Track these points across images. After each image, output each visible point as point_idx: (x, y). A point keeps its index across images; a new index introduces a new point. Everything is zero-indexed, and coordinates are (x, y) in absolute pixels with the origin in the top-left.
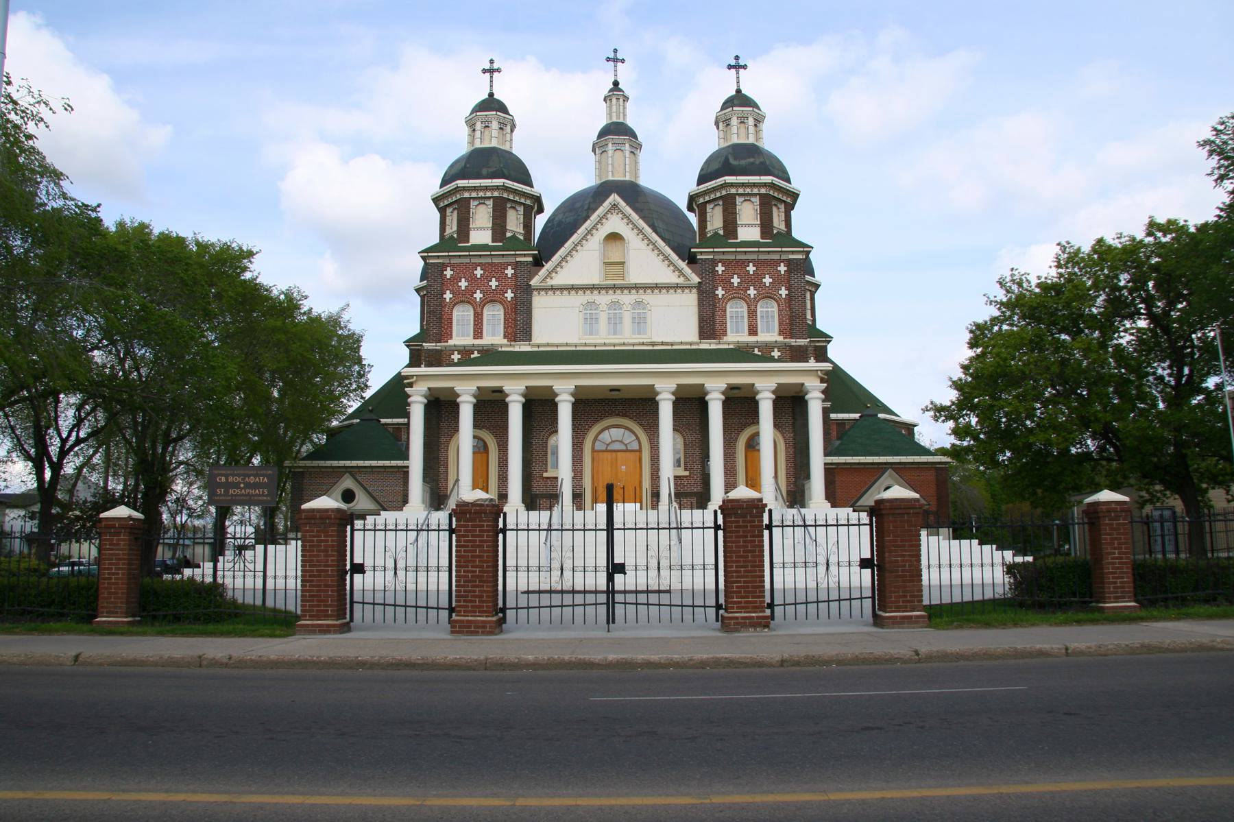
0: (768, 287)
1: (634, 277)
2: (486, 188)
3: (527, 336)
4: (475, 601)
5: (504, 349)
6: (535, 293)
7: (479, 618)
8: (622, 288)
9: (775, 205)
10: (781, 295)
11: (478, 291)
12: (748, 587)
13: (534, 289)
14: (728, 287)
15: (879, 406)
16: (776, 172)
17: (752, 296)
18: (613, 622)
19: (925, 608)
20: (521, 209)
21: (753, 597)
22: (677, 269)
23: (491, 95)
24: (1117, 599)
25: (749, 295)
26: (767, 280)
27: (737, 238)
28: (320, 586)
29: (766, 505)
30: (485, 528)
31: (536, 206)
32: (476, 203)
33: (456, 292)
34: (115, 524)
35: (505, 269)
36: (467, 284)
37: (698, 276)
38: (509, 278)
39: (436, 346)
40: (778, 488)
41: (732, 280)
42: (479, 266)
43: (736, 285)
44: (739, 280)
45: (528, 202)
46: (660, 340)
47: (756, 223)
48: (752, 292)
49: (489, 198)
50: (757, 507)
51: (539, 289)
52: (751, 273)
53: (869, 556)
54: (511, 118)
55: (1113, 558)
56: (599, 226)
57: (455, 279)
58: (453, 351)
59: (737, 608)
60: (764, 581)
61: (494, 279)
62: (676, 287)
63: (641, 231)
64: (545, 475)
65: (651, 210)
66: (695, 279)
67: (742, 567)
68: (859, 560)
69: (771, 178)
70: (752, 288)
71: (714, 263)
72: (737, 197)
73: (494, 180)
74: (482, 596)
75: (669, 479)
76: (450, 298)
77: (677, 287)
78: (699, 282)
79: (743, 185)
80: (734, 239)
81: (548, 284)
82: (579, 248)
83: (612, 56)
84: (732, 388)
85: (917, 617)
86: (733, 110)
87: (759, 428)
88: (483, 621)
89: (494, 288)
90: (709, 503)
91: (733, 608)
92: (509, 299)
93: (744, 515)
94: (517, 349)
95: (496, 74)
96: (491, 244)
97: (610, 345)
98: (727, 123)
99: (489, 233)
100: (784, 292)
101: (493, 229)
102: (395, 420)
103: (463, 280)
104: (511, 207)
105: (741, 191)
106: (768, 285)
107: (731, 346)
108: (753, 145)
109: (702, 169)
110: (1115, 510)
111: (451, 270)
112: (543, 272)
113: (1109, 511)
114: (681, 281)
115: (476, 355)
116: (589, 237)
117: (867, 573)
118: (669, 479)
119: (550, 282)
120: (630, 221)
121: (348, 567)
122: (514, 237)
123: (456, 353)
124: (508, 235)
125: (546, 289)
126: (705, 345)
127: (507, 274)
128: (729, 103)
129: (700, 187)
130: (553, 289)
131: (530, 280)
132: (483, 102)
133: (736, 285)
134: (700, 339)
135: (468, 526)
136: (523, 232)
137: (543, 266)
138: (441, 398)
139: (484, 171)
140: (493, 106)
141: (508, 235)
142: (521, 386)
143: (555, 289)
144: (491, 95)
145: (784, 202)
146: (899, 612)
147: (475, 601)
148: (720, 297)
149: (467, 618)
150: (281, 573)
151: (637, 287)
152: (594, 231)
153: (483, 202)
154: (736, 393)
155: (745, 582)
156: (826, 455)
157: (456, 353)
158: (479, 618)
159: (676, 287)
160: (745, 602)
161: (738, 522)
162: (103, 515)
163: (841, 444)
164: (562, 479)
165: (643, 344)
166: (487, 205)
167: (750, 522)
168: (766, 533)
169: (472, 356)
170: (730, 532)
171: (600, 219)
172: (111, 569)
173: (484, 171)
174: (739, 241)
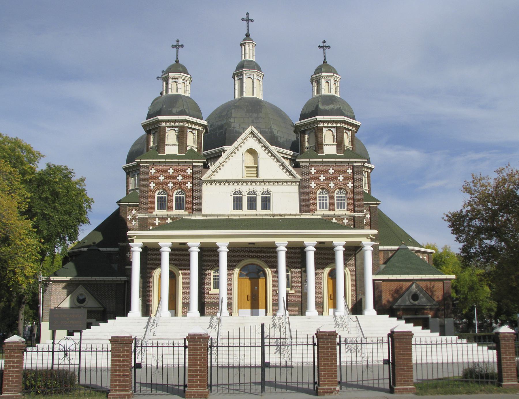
0: (341, 182)
4: (197, 382)
5: (186, 217)
7: (199, 391)
9: (345, 132)
10: (349, 187)
11: (171, 183)
12: (329, 374)
13: (204, 182)
14: (318, 182)
15: (410, 241)
16: (346, 113)
17: (332, 187)
18: (264, 391)
19: (415, 384)
20: (195, 132)
21: (331, 379)
22: (288, 171)
23: (177, 62)
25: (330, 186)
26: (341, 178)
27: (323, 153)
28: (120, 375)
29: (338, 334)
30: (202, 349)
31: (204, 130)
33: (157, 182)
34: (13, 345)
36: (164, 178)
37: (300, 176)
38: (189, 175)
39: (145, 215)
40: (346, 304)
41: (320, 178)
42: (171, 167)
43: (322, 180)
44: (343, 178)
45: (200, 128)
46: (278, 213)
47: (334, 143)
48: (332, 185)
50: (333, 335)
51: (207, 182)
52: (331, 173)
53: (387, 358)
54: (190, 76)
55: (506, 360)
56: (242, 145)
57: (157, 175)
59: (324, 384)
60: (336, 361)
61: (180, 176)
62: (287, 182)
64: (210, 292)
65: (269, 118)
66: (299, 177)
67: (326, 364)
68: (382, 360)
69: (344, 117)
70: (332, 182)
71: (310, 168)
72: (323, 128)
73: (180, 116)
74: (201, 380)
75: (283, 298)
76: (154, 187)
77: (288, 182)
78: (301, 179)
79: (327, 122)
80: (321, 153)
81: (212, 179)
82: (230, 157)
83: (245, 17)
84: (320, 243)
85: (410, 389)
86: (321, 75)
87: (335, 266)
88: (201, 392)
89: (180, 181)
90: (307, 311)
91: (322, 384)
92: (189, 188)
93: (327, 339)
94: (194, 218)
95: (180, 49)
96: (178, 154)
97: (248, 215)
98: (319, 82)
99: (177, 148)
100: (350, 185)
102: (109, 249)
103: (161, 176)
104: (190, 132)
105: (326, 125)
106: (341, 180)
107: (320, 217)
108: (333, 96)
109: (303, 110)
110: (507, 337)
111: (154, 170)
112: (209, 172)
113: (504, 337)
114: (290, 178)
115: (169, 221)
116: (236, 151)
118: (283, 298)
119: (213, 178)
120: (261, 142)
121: (133, 365)
122: (191, 150)
123: (157, 219)
124: (188, 148)
125: (211, 182)
126: (304, 216)
127: (188, 173)
128: (319, 70)
129: (302, 121)
130: (215, 182)
131: (202, 177)
132: (172, 66)
133: (322, 180)
134: (300, 212)
135: (194, 345)
136: (197, 147)
137: (209, 168)
138: (148, 247)
139: (174, 110)
140: (179, 69)
141: (188, 148)
143: (216, 182)
144: (177, 62)
145: (351, 130)
146: (402, 386)
147: (197, 382)
148: (313, 187)
149: (193, 390)
151: (264, 182)
152: (239, 147)
153: (173, 128)
154: (321, 245)
155: (328, 371)
156: (373, 274)
157: (157, 219)
158: (199, 391)
159: (287, 182)
160: (328, 381)
161: (324, 342)
162: (7, 340)
163: (385, 267)
164: (222, 298)
165: (268, 215)
167: (330, 342)
168: (338, 347)
169: (167, 221)
170: (320, 347)
171: (243, 141)
174: (324, 154)
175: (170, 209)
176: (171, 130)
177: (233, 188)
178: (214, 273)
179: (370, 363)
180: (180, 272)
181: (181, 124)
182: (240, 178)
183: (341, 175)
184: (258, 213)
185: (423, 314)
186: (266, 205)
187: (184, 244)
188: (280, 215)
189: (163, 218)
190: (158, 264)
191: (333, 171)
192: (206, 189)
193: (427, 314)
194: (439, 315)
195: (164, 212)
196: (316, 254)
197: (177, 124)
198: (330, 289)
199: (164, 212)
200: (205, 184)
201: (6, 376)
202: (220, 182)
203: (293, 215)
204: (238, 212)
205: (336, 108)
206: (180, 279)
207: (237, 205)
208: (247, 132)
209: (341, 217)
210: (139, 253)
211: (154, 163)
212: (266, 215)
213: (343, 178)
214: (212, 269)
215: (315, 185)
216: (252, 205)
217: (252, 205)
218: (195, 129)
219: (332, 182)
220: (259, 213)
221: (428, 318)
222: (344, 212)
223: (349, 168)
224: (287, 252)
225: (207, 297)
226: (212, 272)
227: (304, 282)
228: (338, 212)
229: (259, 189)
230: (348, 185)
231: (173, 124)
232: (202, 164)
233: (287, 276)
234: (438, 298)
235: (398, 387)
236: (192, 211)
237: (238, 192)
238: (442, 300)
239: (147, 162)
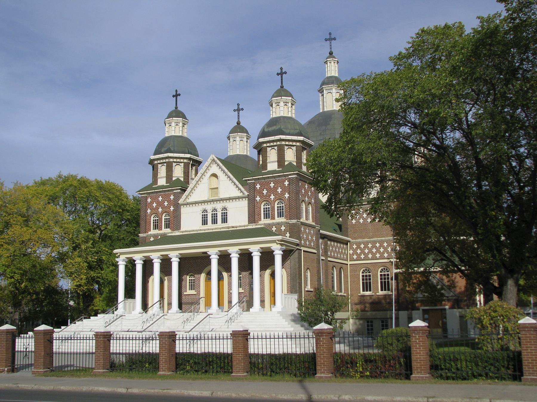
1: (222, 196)
2: (273, 141)
3: (178, 227)
5: (170, 235)
6: (182, 206)
8: (216, 201)
17: (272, 199)
20: (294, 148)
24: (238, 372)
26: (279, 190)
32: (176, 164)
35: (284, 182)
44: (281, 190)
45: (185, 161)
49: (182, 162)
51: (183, 205)
58: (151, 236)
62: (239, 198)
63: (224, 172)
82: (199, 182)
96: (277, 170)
97: (210, 229)
101: (278, 161)
107: (262, 226)
115: (152, 239)
117: (91, 346)
119: (188, 201)
122: (178, 179)
134: (249, 222)
139: (163, 150)
142: (236, 248)
150: (57, 347)
159: (239, 198)
172: (533, 371)
173: (163, 150)
175: (273, 218)
176: (272, 149)
177: (200, 208)
178: (190, 277)
179: (137, 352)
180: (166, 278)
181: (278, 143)
182: (206, 198)
183: (279, 188)
184: (209, 228)
185: (441, 305)
186: (225, 220)
187: (206, 253)
188: (233, 227)
189: (155, 236)
190: (152, 273)
191: (274, 185)
192: (184, 210)
193: (445, 305)
194: (462, 306)
195: (156, 232)
196: (180, 264)
197: (275, 144)
198: (271, 287)
199: (156, 232)
200: (182, 206)
201: (234, 359)
202: (196, 203)
203: (242, 226)
204: (205, 227)
205: (277, 128)
206: (166, 283)
207: (205, 222)
208: (209, 160)
209: (279, 225)
210: (159, 264)
211: (149, 193)
212: (222, 228)
213: (281, 190)
214: (187, 275)
215: (260, 199)
216: (215, 221)
217: (215, 221)
218: (294, 146)
219: (272, 195)
220: (220, 226)
221: (445, 309)
222: (283, 220)
223: (286, 181)
224: (239, 259)
225: (183, 297)
226: (188, 277)
227: (251, 284)
228: (278, 220)
229: (219, 206)
230: (285, 196)
231: (272, 144)
233: (240, 278)
234: (460, 288)
235: (319, 375)
236: (173, 229)
237: (205, 211)
238: (464, 291)
239: (144, 194)
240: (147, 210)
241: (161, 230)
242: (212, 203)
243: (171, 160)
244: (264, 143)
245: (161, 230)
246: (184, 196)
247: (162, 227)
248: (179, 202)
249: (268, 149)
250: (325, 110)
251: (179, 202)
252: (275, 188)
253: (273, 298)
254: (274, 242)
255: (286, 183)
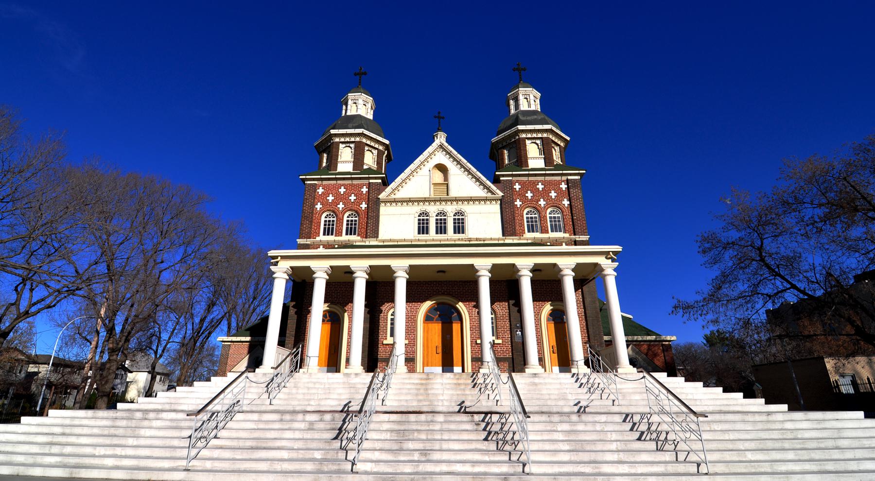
3: (375, 235)
6: (383, 204)
33: (325, 203)
35: (361, 188)
51: (385, 202)
82: (415, 173)
166: (373, 153)
176: (347, 146)
177: (417, 209)
192: (384, 210)
200: (383, 204)
202: (403, 201)
207: (423, 229)
217: (441, 229)
229: (451, 209)
232: (380, 181)
240: (314, 205)
241: (341, 235)
242: (438, 203)
243: (364, 140)
244: (336, 135)
245: (341, 235)
246: (389, 189)
247: (342, 232)
248: (380, 197)
249: (341, 146)
250: (348, 114)
251: (380, 197)
252: (347, 194)
253: (151, 387)
254: (606, 254)
255: (365, 190)
